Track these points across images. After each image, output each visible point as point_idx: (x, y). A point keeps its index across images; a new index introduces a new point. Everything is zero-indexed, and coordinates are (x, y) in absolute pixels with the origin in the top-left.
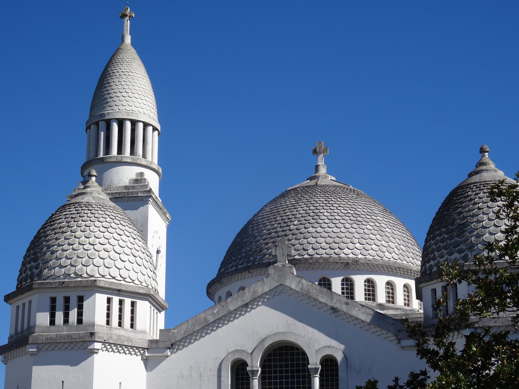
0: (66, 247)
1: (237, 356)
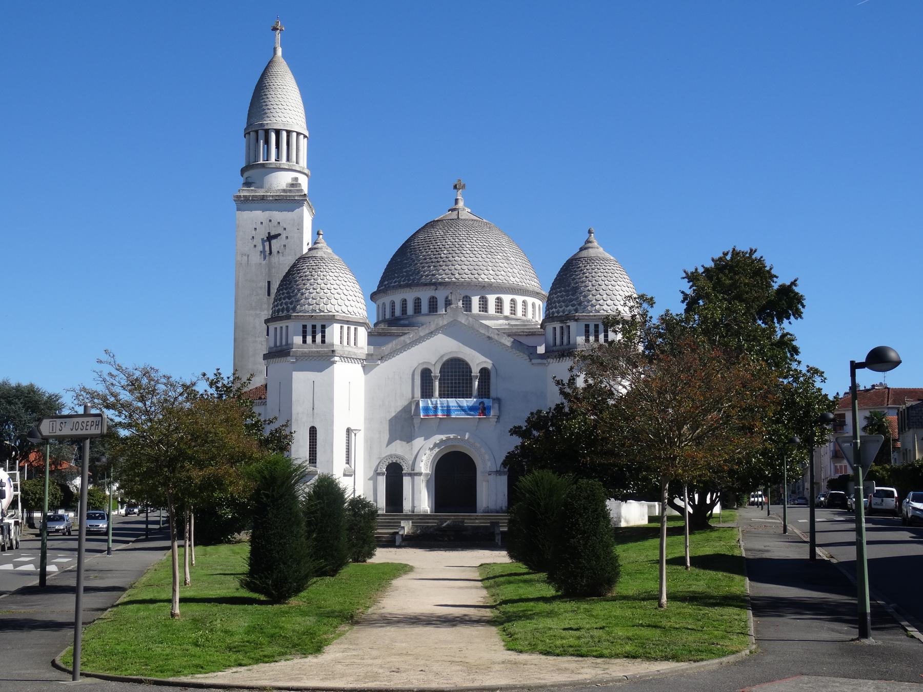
0: (311, 290)
1: (425, 366)
